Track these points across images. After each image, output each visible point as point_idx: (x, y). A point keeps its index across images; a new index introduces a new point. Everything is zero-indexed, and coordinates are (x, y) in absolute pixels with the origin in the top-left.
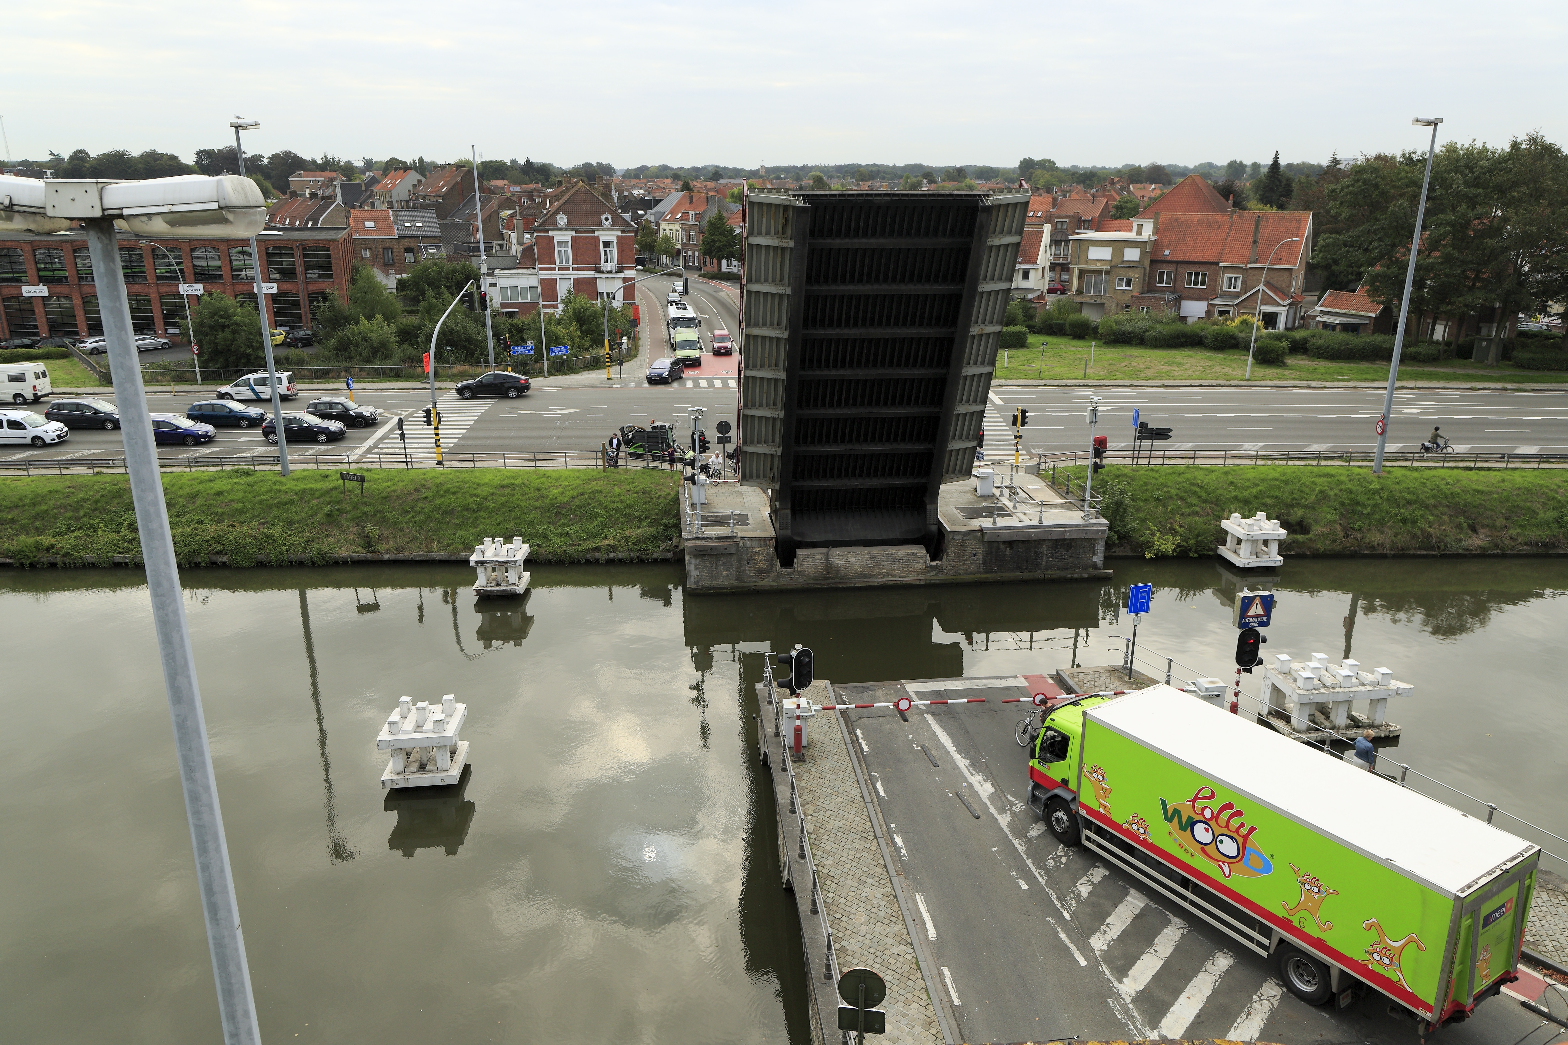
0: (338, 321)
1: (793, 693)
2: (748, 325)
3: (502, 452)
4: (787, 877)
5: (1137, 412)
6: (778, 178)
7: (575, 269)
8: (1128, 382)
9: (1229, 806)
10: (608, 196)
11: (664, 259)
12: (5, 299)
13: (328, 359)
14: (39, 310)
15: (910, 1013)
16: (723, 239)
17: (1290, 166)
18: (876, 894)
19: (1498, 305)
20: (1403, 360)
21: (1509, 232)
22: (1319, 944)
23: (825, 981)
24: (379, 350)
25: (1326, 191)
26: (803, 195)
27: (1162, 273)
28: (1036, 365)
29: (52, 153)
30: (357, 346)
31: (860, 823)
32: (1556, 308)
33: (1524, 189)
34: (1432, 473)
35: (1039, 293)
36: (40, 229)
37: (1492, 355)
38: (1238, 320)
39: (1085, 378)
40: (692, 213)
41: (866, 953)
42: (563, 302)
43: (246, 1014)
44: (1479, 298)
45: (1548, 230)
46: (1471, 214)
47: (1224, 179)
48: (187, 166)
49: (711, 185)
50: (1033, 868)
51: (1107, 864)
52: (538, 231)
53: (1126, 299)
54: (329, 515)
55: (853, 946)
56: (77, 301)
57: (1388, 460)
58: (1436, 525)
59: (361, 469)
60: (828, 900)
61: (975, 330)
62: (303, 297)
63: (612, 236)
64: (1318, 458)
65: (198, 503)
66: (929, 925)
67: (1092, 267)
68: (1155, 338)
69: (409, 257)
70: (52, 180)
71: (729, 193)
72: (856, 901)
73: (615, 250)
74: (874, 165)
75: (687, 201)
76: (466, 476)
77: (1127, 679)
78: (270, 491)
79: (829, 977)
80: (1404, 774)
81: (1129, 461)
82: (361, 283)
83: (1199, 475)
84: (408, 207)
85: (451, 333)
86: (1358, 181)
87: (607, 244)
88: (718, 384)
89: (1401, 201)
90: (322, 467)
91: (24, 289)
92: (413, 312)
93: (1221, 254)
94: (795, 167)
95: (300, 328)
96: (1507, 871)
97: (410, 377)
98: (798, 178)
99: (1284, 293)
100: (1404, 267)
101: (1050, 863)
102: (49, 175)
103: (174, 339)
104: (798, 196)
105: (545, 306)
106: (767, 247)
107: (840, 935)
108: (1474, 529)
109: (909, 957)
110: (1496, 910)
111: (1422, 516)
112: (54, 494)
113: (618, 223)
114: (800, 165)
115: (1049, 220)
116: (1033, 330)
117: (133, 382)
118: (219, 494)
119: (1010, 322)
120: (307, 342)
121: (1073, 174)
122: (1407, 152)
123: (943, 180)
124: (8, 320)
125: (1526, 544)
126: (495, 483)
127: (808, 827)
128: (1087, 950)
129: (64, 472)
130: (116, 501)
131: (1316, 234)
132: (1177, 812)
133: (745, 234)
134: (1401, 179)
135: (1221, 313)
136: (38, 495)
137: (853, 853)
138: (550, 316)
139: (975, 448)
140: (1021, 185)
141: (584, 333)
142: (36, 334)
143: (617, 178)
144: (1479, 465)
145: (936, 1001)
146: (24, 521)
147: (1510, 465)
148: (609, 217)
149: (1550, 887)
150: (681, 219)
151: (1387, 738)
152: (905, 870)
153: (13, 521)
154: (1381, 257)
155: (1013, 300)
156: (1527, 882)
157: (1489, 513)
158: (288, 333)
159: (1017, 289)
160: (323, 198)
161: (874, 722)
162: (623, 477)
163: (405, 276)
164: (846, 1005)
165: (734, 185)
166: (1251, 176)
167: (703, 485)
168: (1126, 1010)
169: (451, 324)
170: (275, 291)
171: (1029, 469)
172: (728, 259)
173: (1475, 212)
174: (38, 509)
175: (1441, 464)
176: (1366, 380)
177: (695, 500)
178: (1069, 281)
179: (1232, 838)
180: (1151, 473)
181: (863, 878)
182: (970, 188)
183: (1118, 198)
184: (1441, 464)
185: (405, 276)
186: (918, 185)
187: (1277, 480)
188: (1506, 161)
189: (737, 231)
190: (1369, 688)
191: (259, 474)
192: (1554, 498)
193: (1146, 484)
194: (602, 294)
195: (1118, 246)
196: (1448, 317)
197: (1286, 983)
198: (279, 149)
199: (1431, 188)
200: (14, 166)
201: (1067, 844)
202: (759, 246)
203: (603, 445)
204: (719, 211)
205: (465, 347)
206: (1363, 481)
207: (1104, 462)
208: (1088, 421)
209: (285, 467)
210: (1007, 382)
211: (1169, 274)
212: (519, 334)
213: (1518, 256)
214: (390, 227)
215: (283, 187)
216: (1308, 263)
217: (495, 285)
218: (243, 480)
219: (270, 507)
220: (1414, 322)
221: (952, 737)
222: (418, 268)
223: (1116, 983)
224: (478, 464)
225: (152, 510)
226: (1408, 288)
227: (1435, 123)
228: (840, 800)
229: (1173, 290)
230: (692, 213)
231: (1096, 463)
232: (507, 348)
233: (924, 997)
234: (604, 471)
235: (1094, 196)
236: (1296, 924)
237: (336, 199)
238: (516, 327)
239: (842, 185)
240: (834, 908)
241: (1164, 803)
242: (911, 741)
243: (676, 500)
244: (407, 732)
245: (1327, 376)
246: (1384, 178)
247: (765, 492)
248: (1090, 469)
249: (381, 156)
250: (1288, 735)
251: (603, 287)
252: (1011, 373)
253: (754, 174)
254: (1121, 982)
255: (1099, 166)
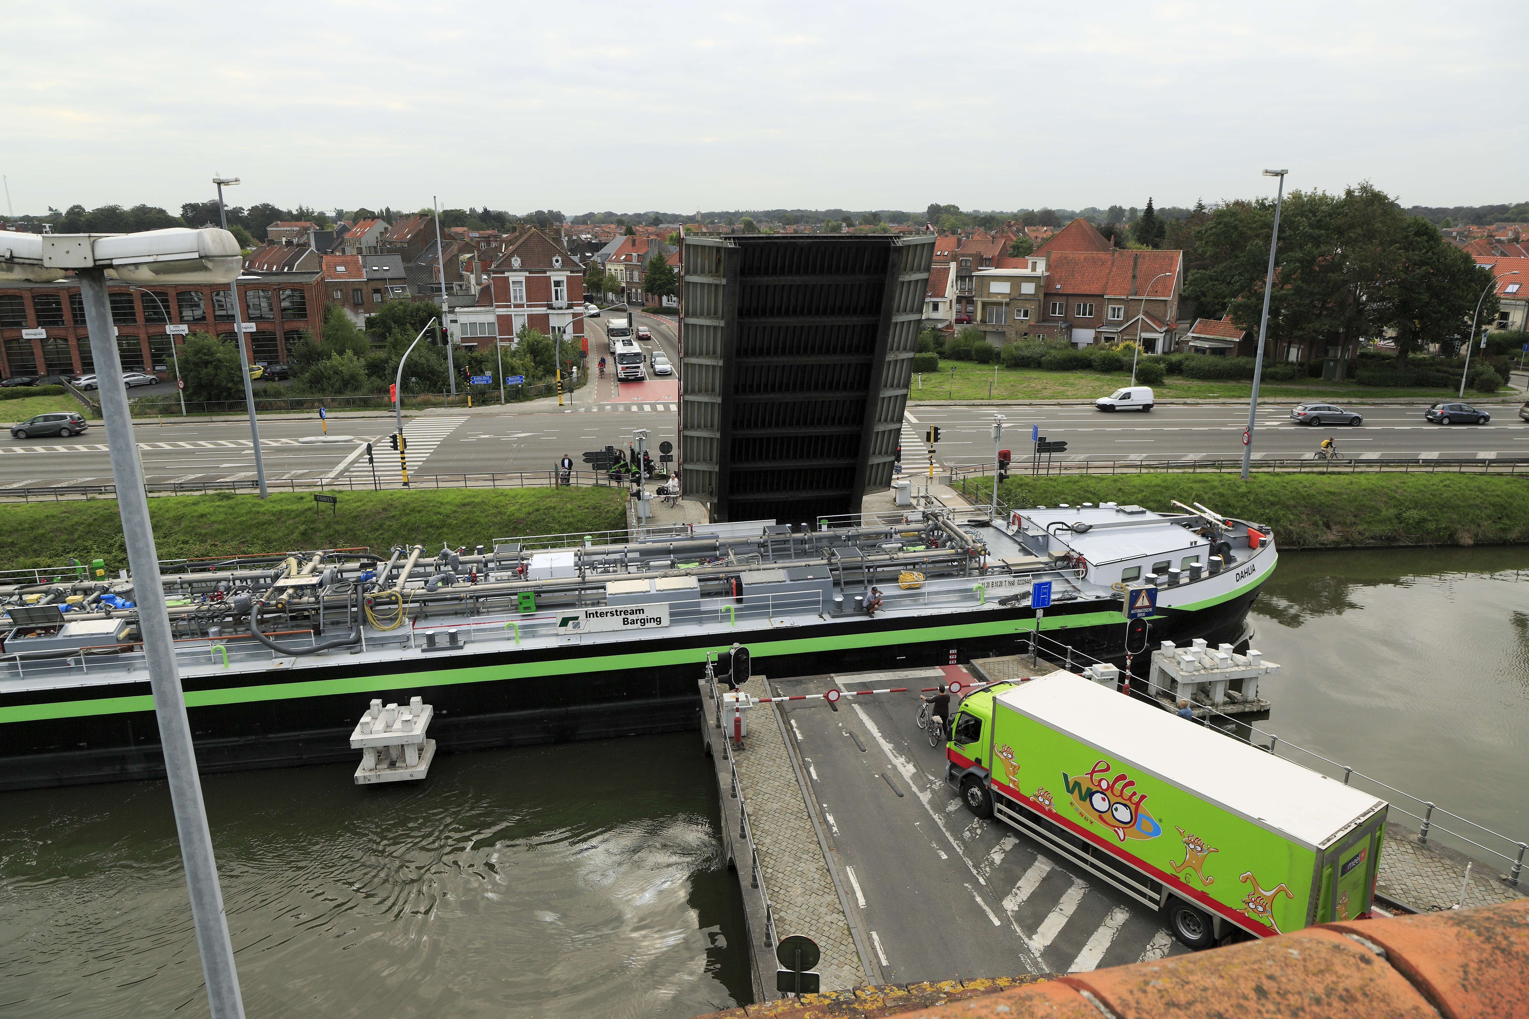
0: (311, 356)
1: (732, 688)
2: (686, 354)
3: (462, 473)
4: (729, 855)
5: (1036, 428)
6: (713, 223)
7: (528, 306)
8: (1028, 402)
9: (1122, 777)
10: (558, 240)
11: (610, 296)
12: (7, 342)
13: (303, 391)
14: (38, 351)
15: (843, 974)
16: (663, 277)
17: (1162, 210)
18: (810, 868)
19: (1341, 330)
20: (1263, 379)
21: (1348, 268)
22: (1203, 897)
23: (765, 949)
24: (349, 382)
25: (1193, 233)
26: (734, 238)
27: (1054, 305)
28: (947, 387)
29: (51, 209)
30: (329, 379)
31: (795, 804)
32: (1390, 332)
33: (1359, 230)
34: (1288, 478)
35: (947, 323)
36: (38, 279)
37: (1338, 373)
38: (1121, 345)
39: (990, 398)
40: (634, 254)
41: (802, 922)
42: (518, 336)
43: (231, 990)
44: (1325, 325)
45: (1381, 265)
46: (1316, 252)
47: (1106, 222)
48: (174, 219)
49: (652, 229)
50: (951, 839)
51: (1017, 834)
52: (495, 272)
53: (1024, 328)
54: (304, 534)
55: (790, 916)
56: (72, 342)
57: (1254, 467)
58: (1296, 523)
59: (333, 491)
60: (768, 875)
61: (890, 357)
62: (279, 335)
63: (562, 276)
64: (1194, 466)
65: (183, 525)
66: (859, 894)
67: (994, 299)
68: (1051, 362)
69: (377, 297)
70: (50, 235)
71: (668, 236)
72: (793, 876)
73: (565, 289)
74: (799, 211)
75: (631, 243)
76: (430, 496)
77: (1032, 667)
78: (250, 512)
79: (769, 945)
80: (1273, 743)
81: (1030, 472)
82: (332, 322)
83: (1092, 483)
84: (376, 252)
85: (415, 366)
86: (1220, 223)
87: (558, 284)
88: (660, 408)
89: (1257, 241)
90: (297, 490)
91: (24, 332)
92: (380, 347)
93: (1105, 287)
94: (728, 213)
95: (277, 363)
96: (1360, 825)
97: (377, 406)
98: (730, 223)
99: (1160, 322)
100: (1261, 298)
101: (967, 834)
102: (48, 229)
103: (160, 375)
104: (730, 238)
105: (502, 340)
106: (702, 285)
107: (779, 906)
108: (1328, 526)
109: (841, 924)
110: (1352, 860)
111: (1284, 515)
112: (50, 519)
113: (567, 264)
114: (732, 210)
115: (954, 258)
116: (943, 356)
117: (121, 414)
118: (202, 516)
119: (922, 348)
120: (283, 376)
121: (975, 218)
122: (1260, 198)
123: (860, 224)
124: (9, 361)
125: (1372, 538)
126: (457, 501)
127: (748, 809)
128: (1000, 911)
129: (60, 498)
130: (107, 524)
131: (1186, 269)
132: (1077, 784)
133: (682, 273)
134: (1255, 222)
135: (1107, 339)
136: (36, 520)
137: (789, 831)
138: (506, 349)
139: (893, 462)
140: (928, 228)
141: (538, 364)
142: (35, 373)
143: (566, 225)
144: (1330, 469)
145: (866, 962)
146: (23, 544)
147: (1357, 470)
148: (560, 259)
149: (1398, 837)
150: (625, 260)
151: (1259, 712)
152: (836, 845)
153: (13, 544)
154: (1242, 289)
155: (924, 329)
156: (1378, 834)
157: (1340, 512)
158: (266, 368)
159: (928, 319)
160: (298, 245)
161: (807, 712)
162: (574, 494)
163: (373, 314)
164: (784, 970)
165: (673, 229)
166: (1130, 219)
167: (648, 500)
168: (1035, 964)
169: (415, 357)
170: (254, 330)
171: (942, 480)
172: (668, 294)
173: (1320, 250)
174: (36, 532)
175: (1298, 470)
176: (1233, 397)
177: (641, 514)
178: (974, 312)
179: (1125, 805)
180: (1050, 482)
181: (799, 854)
182: (885, 230)
183: (1015, 239)
184: (1298, 470)
185: (373, 314)
186: (838, 228)
187: (1159, 486)
188: (1343, 207)
189: (676, 270)
190: (1242, 668)
191: (239, 497)
192: (1394, 498)
193: (1045, 492)
194: (554, 328)
195: (1016, 281)
196: (1301, 340)
197: (1175, 933)
198: (258, 202)
199: (1281, 229)
200: (16, 221)
201: (982, 817)
202: (695, 284)
203: (556, 466)
204: (659, 253)
205: (428, 379)
206: (1233, 486)
207: (1009, 472)
208: (993, 436)
209: (263, 490)
210: (921, 403)
211: (1061, 306)
212: (478, 366)
213: (1356, 288)
214: (359, 270)
215: (262, 236)
216: (1180, 295)
217: (456, 321)
218: (224, 503)
219: (250, 527)
220: (1272, 346)
221: (877, 724)
222: (385, 307)
223: (1026, 940)
224: (441, 484)
225: (139, 530)
226: (1265, 316)
227: (1281, 174)
228: (777, 784)
229: (1065, 320)
230: (634, 254)
231: (1001, 474)
232: (467, 378)
233: (855, 959)
234: (557, 488)
235: (993, 237)
236: (1182, 880)
237: (309, 246)
238: (475, 359)
239: (770, 228)
240: (773, 882)
241: (1065, 776)
242: (841, 729)
243: (624, 514)
244: (377, 732)
245: (1200, 394)
246: (1241, 221)
247: (704, 505)
248: (996, 479)
249: (352, 207)
250: (1173, 713)
251: (555, 321)
252: (924, 395)
253: (691, 219)
254: (1030, 938)
255: (998, 210)
